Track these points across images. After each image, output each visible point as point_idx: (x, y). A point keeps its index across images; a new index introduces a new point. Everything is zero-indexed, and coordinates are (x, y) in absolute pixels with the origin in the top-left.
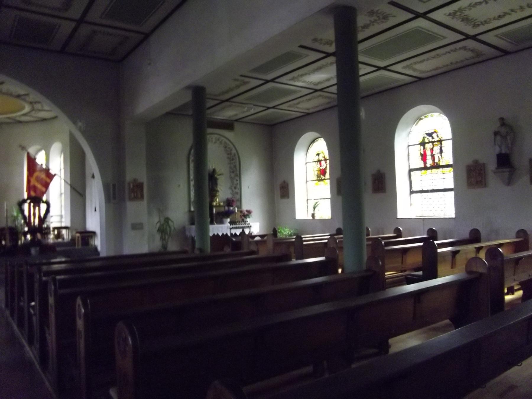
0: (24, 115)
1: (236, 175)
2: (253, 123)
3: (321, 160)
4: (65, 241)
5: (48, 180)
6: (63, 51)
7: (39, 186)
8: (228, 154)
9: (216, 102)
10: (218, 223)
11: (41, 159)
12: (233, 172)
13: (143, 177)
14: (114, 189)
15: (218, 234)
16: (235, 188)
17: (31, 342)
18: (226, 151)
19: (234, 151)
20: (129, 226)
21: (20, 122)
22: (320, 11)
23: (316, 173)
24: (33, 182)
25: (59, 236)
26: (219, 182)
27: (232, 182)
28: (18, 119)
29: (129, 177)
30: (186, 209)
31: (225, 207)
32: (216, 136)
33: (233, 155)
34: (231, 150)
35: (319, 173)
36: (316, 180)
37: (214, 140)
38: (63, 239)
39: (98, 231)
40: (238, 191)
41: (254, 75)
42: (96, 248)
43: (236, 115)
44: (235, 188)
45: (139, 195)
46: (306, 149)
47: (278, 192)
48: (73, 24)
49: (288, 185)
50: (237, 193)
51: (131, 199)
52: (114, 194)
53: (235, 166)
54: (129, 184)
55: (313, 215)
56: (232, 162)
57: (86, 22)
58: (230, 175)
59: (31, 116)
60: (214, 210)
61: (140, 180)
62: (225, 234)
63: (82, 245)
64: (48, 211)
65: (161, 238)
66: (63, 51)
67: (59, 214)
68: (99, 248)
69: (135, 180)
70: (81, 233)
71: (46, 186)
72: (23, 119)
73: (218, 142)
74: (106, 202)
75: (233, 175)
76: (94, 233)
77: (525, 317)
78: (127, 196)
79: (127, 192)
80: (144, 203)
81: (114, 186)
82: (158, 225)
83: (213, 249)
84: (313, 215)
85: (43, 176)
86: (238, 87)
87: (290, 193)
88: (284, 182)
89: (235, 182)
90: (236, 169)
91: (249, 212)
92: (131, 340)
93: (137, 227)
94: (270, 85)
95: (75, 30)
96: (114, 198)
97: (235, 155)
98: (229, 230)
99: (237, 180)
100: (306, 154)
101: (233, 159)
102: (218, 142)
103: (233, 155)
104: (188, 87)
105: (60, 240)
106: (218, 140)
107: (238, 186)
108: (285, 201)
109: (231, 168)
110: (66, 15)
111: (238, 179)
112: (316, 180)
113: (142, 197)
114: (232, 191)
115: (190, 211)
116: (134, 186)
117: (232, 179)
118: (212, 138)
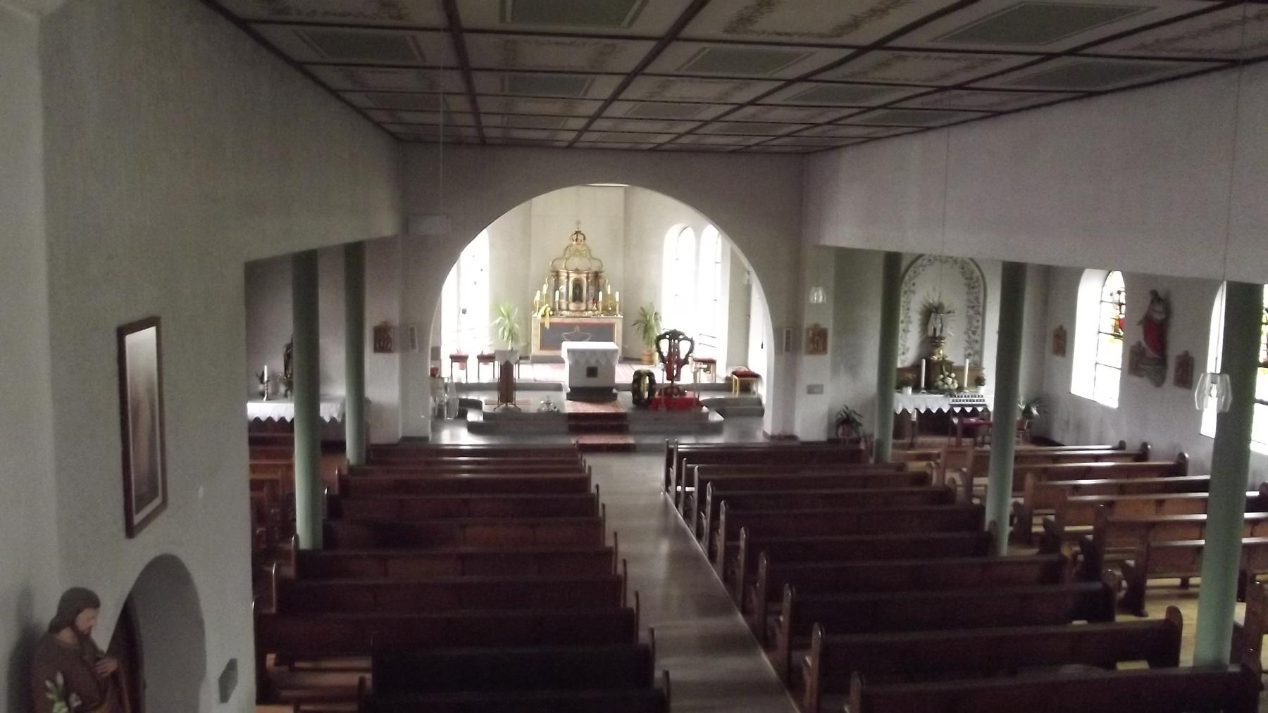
1: (978, 313)
3: (1123, 304)
8: (967, 279)
12: (973, 307)
13: (828, 323)
14: (788, 338)
16: (974, 333)
17: (699, 536)
18: (963, 274)
19: (977, 273)
23: (1113, 322)
27: (970, 322)
29: (809, 321)
33: (975, 279)
34: (972, 273)
35: (1117, 323)
36: (1112, 334)
39: (763, 373)
40: (977, 337)
42: (759, 402)
44: (974, 333)
45: (821, 348)
50: (977, 342)
52: (787, 344)
53: (977, 299)
54: (808, 330)
56: (972, 290)
58: (968, 312)
61: (823, 326)
68: (764, 401)
69: (816, 326)
75: (971, 312)
76: (757, 376)
77: (274, 595)
80: (827, 358)
81: (788, 333)
87: (1067, 349)
88: (1061, 328)
89: (975, 324)
90: (978, 303)
92: (764, 661)
96: (787, 350)
97: (978, 280)
99: (978, 321)
101: (974, 287)
103: (975, 279)
107: (979, 331)
108: (1058, 358)
109: (969, 300)
111: (980, 320)
112: (1112, 334)
113: (824, 350)
114: (969, 337)
116: (813, 334)
117: (970, 319)
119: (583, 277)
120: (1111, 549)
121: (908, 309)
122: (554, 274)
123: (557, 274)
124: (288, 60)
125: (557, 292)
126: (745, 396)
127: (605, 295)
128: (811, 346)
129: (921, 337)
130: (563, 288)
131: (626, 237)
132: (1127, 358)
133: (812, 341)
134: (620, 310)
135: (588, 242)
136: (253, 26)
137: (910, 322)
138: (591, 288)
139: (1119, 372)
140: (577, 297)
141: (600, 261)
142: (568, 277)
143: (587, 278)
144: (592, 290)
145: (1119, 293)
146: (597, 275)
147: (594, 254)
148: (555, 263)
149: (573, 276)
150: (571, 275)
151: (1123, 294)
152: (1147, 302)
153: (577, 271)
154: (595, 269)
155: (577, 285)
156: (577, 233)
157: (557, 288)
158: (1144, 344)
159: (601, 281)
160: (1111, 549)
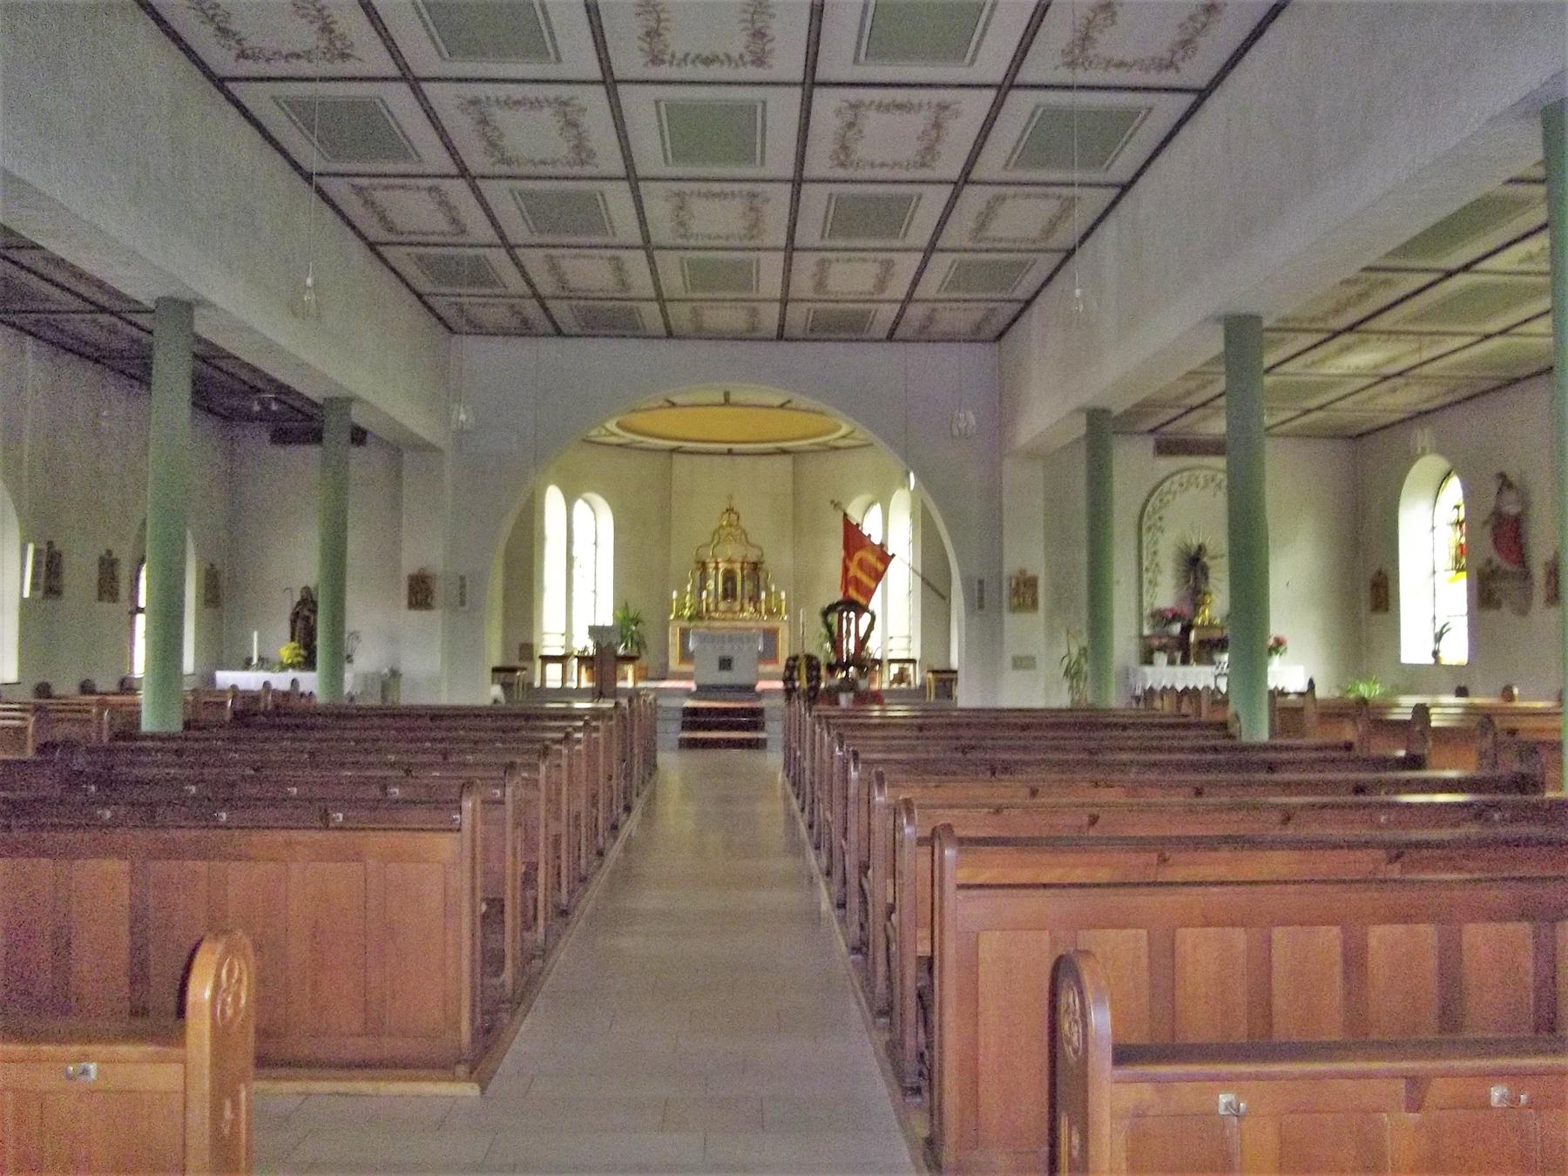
0: (844, 437)
2: (1307, 435)
4: (913, 686)
5: (880, 567)
6: (890, 337)
7: (865, 579)
9: (1182, 411)
10: (1199, 661)
11: (871, 526)
15: (1173, 688)
20: (1008, 662)
21: (837, 448)
22: (1206, 320)
23: (1453, 551)
24: (854, 570)
25: (901, 677)
26: (1212, 574)
28: (831, 443)
29: (1010, 566)
30: (1133, 632)
31: (1222, 628)
32: (1205, 472)
37: (1201, 481)
38: (909, 683)
41: (1403, 263)
43: (1393, 360)
45: (1029, 601)
46: (1432, 493)
47: (1365, 595)
48: (897, 307)
49: (1386, 578)
51: (1015, 609)
55: (1435, 654)
57: (1018, 86)
59: (854, 438)
60: (1193, 636)
61: (1030, 573)
62: (1191, 687)
63: (937, 696)
64: (871, 627)
65: (1071, 687)
66: (890, 337)
67: (907, 633)
70: (934, 672)
71: (878, 576)
72: (842, 443)
73: (1212, 485)
74: (967, 616)
78: (1006, 604)
79: (1006, 592)
82: (1066, 661)
83: (1273, 734)
84: (1435, 654)
85: (872, 559)
86: (1363, 296)
88: (1380, 573)
91: (1279, 643)
93: (1024, 663)
94: (1462, 280)
95: (900, 316)
98: (1213, 679)
100: (1432, 502)
102: (1212, 485)
104: (1079, 410)
105: (904, 686)
106: (1213, 480)
108: (1379, 617)
110: (882, 297)
113: (1034, 604)
115: (1141, 636)
116: (1018, 584)
118: (1197, 478)
119: (737, 567)
120: (1452, 711)
121: (1155, 553)
122: (700, 565)
123: (703, 565)
124: (296, 166)
125: (704, 594)
126: (945, 703)
127: (769, 594)
128: (1015, 601)
129: (1177, 593)
130: (711, 584)
131: (796, 519)
132: (1475, 591)
133: (1016, 592)
134: (786, 612)
135: (742, 523)
136: (230, 86)
137: (1160, 572)
138: (746, 583)
139: (1466, 618)
140: (729, 594)
141: (760, 548)
142: (717, 568)
143: (742, 569)
144: (749, 586)
145: (1458, 507)
146: (756, 567)
147: (753, 538)
148: (700, 550)
149: (722, 566)
150: (720, 565)
151: (1462, 509)
152: (1493, 487)
153: (730, 561)
154: (752, 558)
155: (729, 577)
156: (730, 510)
157: (703, 587)
158: (1497, 559)
159: (762, 575)
160: (1452, 711)
